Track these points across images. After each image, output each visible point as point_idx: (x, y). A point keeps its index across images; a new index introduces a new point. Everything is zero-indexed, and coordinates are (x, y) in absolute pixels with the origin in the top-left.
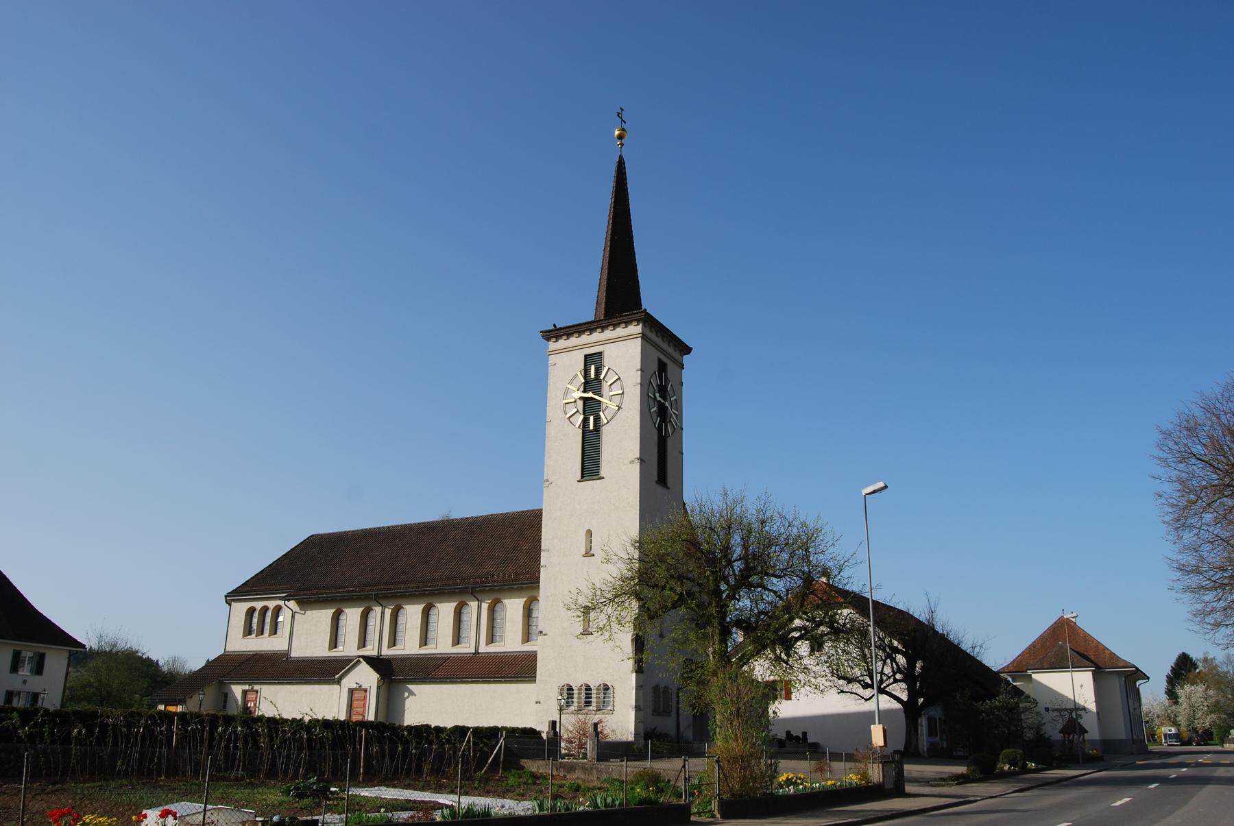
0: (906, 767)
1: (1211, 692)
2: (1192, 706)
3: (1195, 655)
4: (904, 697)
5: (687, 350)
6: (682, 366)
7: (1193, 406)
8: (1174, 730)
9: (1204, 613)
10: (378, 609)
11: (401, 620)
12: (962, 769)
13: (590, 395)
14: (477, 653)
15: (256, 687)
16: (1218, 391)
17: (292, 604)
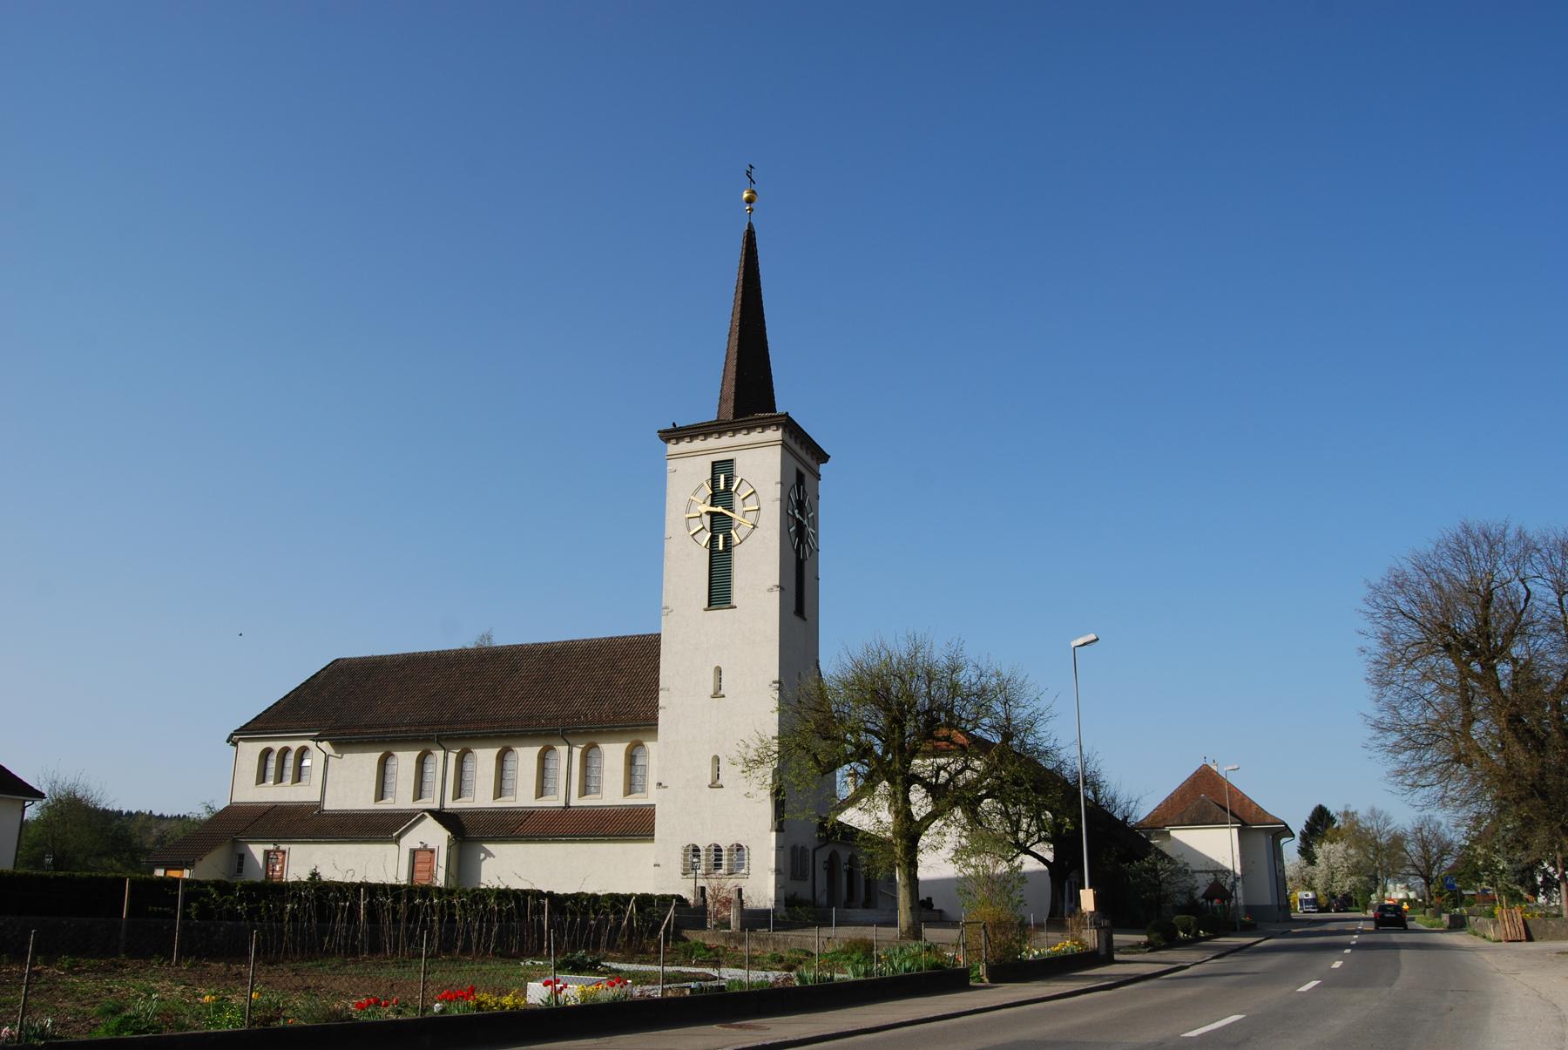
0: (1116, 937)
1: (1352, 851)
2: (1330, 867)
3: (1334, 808)
4: (1049, 856)
5: (823, 457)
6: (818, 477)
7: (1403, 562)
8: (1311, 895)
9: (1401, 773)
10: (440, 754)
11: (468, 767)
12: (1143, 938)
13: (720, 509)
14: (567, 806)
15: (283, 847)
16: (1431, 547)
17: (325, 745)
